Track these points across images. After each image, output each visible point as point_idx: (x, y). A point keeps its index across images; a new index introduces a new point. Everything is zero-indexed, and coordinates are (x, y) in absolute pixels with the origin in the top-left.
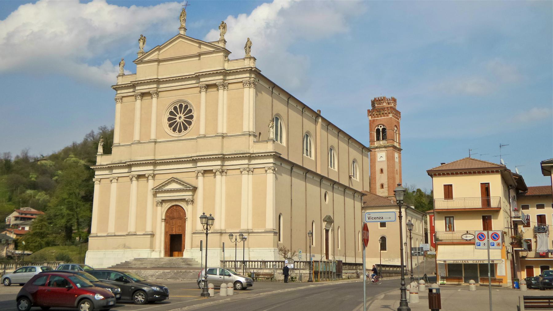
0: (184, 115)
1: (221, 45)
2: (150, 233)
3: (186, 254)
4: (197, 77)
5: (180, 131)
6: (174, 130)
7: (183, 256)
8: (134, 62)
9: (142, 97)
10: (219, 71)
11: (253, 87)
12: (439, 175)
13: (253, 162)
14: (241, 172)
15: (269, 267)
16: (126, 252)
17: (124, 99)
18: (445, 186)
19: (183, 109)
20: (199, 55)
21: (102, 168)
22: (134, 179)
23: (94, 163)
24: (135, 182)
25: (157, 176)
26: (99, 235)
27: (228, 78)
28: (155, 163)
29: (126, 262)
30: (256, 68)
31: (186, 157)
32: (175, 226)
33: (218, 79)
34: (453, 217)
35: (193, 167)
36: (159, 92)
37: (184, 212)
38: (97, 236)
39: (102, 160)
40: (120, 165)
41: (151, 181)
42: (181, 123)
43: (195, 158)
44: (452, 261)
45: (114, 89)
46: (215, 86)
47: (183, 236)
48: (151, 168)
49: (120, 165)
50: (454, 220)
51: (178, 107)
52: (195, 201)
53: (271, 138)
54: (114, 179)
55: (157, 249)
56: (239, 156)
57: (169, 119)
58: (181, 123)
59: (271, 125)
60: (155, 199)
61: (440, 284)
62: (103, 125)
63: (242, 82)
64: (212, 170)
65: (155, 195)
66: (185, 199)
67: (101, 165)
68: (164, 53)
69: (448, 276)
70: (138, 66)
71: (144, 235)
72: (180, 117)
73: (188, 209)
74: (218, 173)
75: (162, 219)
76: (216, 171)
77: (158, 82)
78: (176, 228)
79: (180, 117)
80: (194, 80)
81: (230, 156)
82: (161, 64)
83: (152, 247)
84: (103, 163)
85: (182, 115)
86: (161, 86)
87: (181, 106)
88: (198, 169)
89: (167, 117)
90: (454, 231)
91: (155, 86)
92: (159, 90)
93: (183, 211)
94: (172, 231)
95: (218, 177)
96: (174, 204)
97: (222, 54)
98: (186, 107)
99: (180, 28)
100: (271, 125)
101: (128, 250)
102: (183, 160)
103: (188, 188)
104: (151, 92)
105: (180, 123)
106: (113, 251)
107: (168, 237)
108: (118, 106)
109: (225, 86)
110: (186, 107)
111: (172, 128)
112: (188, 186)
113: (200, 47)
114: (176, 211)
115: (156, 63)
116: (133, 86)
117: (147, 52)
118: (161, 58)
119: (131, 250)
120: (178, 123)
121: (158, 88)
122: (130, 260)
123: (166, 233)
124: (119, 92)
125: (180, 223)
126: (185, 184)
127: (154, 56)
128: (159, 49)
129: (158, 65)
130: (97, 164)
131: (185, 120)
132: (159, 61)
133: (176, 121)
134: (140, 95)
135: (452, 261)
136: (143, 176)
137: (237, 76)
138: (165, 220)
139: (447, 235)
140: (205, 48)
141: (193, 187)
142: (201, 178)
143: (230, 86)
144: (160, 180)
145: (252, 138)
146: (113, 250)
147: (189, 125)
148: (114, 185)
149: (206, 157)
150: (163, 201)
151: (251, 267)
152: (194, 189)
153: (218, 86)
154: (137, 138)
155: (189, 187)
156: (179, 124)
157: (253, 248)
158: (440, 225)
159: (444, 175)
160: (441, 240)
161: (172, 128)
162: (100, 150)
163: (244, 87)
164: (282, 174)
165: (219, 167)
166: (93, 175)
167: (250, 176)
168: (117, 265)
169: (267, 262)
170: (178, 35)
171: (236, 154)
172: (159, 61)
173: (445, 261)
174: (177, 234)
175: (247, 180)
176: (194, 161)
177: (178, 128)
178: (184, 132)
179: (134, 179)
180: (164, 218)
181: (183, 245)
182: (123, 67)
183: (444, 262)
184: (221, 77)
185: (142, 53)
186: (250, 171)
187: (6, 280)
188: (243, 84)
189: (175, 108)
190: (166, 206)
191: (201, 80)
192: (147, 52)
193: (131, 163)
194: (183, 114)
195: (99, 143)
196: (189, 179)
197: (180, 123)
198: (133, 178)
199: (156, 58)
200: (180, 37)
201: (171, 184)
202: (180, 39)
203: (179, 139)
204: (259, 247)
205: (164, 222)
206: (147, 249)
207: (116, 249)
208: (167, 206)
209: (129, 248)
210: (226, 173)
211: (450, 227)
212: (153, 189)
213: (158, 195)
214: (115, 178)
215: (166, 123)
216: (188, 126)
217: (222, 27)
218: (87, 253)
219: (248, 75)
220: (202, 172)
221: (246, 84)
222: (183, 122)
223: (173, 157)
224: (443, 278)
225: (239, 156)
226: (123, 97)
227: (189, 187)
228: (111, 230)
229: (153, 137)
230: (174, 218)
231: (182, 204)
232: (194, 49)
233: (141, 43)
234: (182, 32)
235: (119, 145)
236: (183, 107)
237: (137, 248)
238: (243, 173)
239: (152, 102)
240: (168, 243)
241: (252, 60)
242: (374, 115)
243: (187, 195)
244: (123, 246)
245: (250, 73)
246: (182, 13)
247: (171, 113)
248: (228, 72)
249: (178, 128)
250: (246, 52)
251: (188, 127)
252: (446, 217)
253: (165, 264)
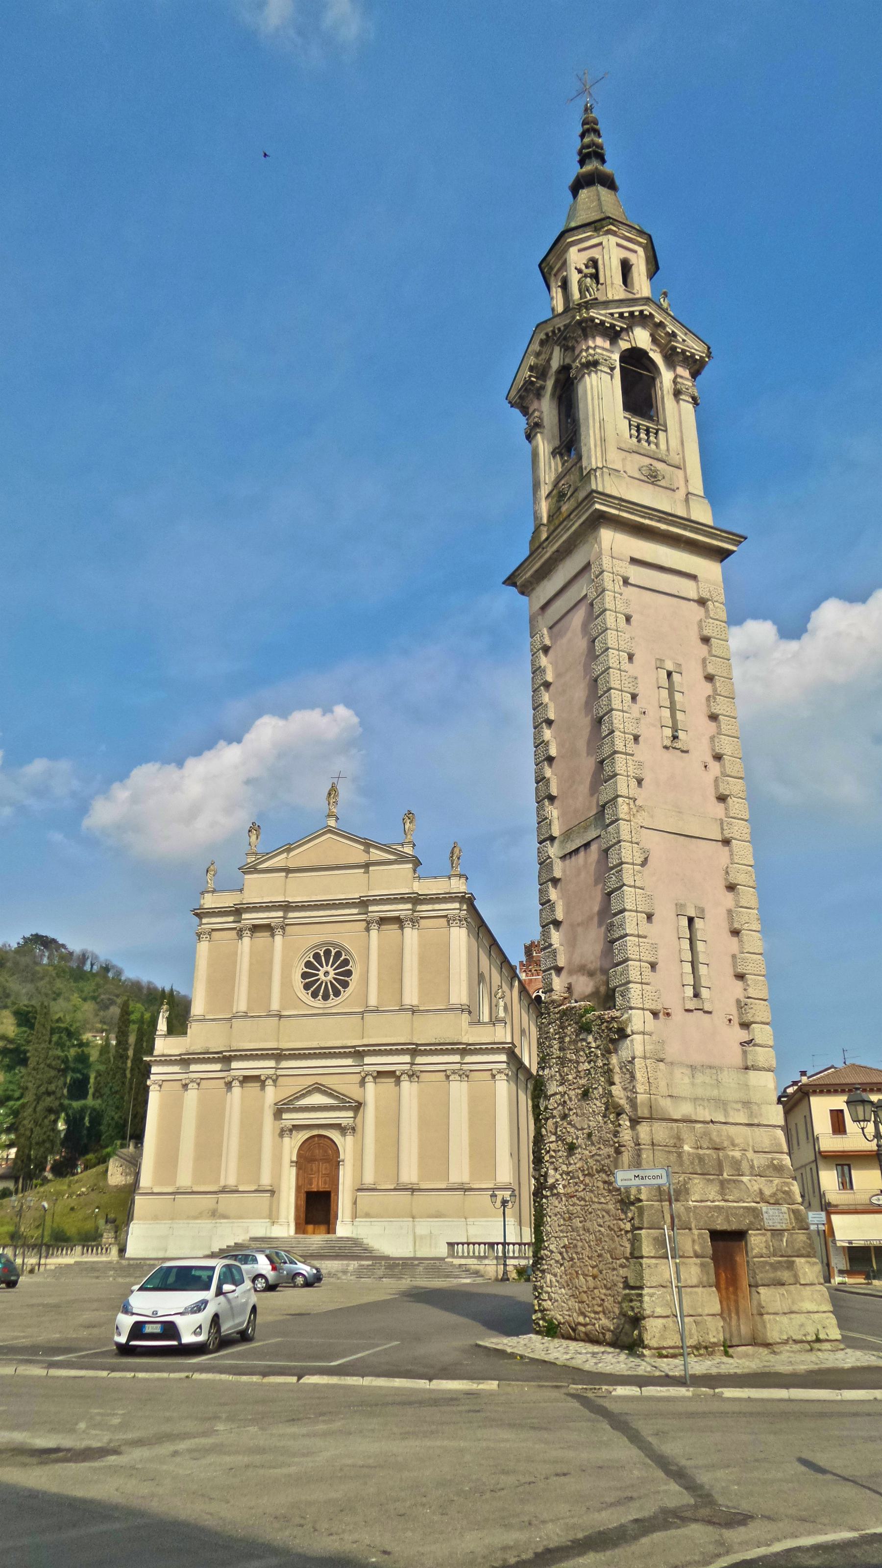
0: (335, 970)
1: (408, 850)
2: (269, 1188)
3: (343, 1229)
4: (363, 904)
5: (326, 997)
6: (315, 995)
7: (335, 1233)
8: (239, 869)
9: (253, 932)
10: (406, 896)
11: (465, 925)
12: (821, 1092)
13: (469, 1059)
14: (448, 1077)
15: (460, 1254)
16: (218, 1225)
17: (214, 933)
18: (831, 1111)
19: (323, 958)
20: (366, 866)
21: (167, 1060)
22: (236, 1083)
23: (150, 1051)
24: (237, 1090)
25: (280, 1078)
26: (155, 1191)
27: (419, 908)
28: (279, 1056)
29: (235, 1244)
30: (472, 894)
31: (340, 1045)
32: (316, 1175)
33: (402, 909)
34: (849, 1166)
35: (354, 1064)
36: (287, 925)
37: (335, 1148)
38: (153, 1194)
39: (163, 1045)
40: (206, 1056)
41: (270, 1089)
42: (329, 984)
43: (361, 1049)
44: (863, 1242)
45: (197, 915)
46: (398, 921)
47: (332, 1195)
48: (272, 1063)
49: (206, 1056)
50: (853, 1172)
51: (322, 953)
52: (359, 1129)
53: (501, 1017)
54: (192, 1081)
55: (282, 1220)
56: (444, 1047)
57: (304, 975)
58: (329, 984)
59: (500, 994)
60: (277, 1122)
61: (839, 1284)
62: (151, 980)
63: (446, 916)
64: (394, 1072)
65: (278, 1114)
66: (340, 1124)
67: (163, 1056)
68: (295, 859)
69: (849, 1269)
70: (247, 877)
71: (256, 1191)
72: (326, 973)
73: (346, 1145)
74: (404, 1077)
75: (292, 1162)
76: (402, 1074)
77: (287, 907)
78: (318, 1180)
79: (326, 973)
80: (355, 907)
81: (428, 1048)
82: (290, 875)
83: (273, 1217)
84: (167, 1052)
85: (329, 969)
86: (291, 915)
87: (327, 953)
88: (366, 1068)
89: (301, 972)
90: (852, 1188)
91: (280, 914)
92: (287, 921)
93: (334, 1146)
94: (311, 1184)
95: (405, 1085)
96: (315, 1132)
97: (411, 866)
98: (338, 955)
99: (329, 816)
100: (500, 994)
101: (222, 1221)
102: (337, 1051)
103: (347, 1105)
104: (272, 925)
105: (326, 983)
106: (189, 1223)
107: (303, 1196)
108: (203, 947)
109: (414, 922)
110: (338, 955)
111: (310, 992)
112: (348, 1100)
113: (368, 853)
114: (319, 1146)
115: (284, 874)
116: (237, 912)
117: (268, 854)
118: (291, 865)
119: (231, 1221)
120: (322, 983)
121: (285, 918)
122: (244, 1241)
123: (298, 1188)
124: (204, 921)
125: (326, 1168)
126: (342, 1097)
127: (278, 861)
128: (289, 850)
129: (286, 877)
130: (156, 1053)
131: (335, 979)
132: (288, 871)
133: (319, 979)
134: (250, 929)
135: (863, 1242)
136: (256, 1078)
137: (437, 907)
138: (297, 1162)
139: (843, 1196)
140: (376, 855)
141: (356, 1102)
142: (370, 1086)
143: (422, 922)
144: (289, 1087)
145: (465, 1015)
146: (188, 1221)
147: (343, 988)
148: (192, 1095)
149: (383, 1048)
150: (297, 1128)
151: (471, 1254)
152: (358, 1107)
153: (403, 922)
154: (242, 1005)
155: (349, 1102)
156: (324, 984)
157: (474, 1217)
158: (829, 1179)
159: (829, 1092)
160: (836, 1206)
161: (310, 992)
162: (162, 1026)
163: (449, 925)
164: (511, 1082)
165: (407, 1067)
166: (147, 1073)
167: (464, 1084)
168: (220, 1250)
169: (458, 1244)
170: (325, 828)
171: (440, 1044)
172: (288, 871)
173: (850, 1242)
174: (321, 1190)
175: (458, 1090)
176: (358, 1054)
177: (322, 991)
178: (333, 1001)
179: (236, 1083)
180: (294, 1159)
181: (332, 1213)
182: (214, 875)
183: (849, 1243)
184: (409, 906)
185: (256, 854)
186: (464, 1075)
187: (260, 1279)
188: (448, 921)
189: (317, 956)
190: (300, 1136)
191: (371, 909)
192: (268, 854)
193: (233, 1054)
194: (331, 967)
195: (161, 1014)
196: (349, 1087)
197: (326, 983)
198: (234, 1082)
199: (282, 864)
200: (330, 831)
201: (311, 1095)
202: (329, 835)
203: (326, 1011)
204: (484, 1217)
205: (295, 1168)
206: (264, 1218)
207: (195, 1218)
208: (302, 1136)
209: (225, 1217)
210: (418, 1077)
211: (846, 1184)
212: (275, 1104)
213: (285, 1116)
214: (195, 1081)
215: (298, 982)
216: (342, 990)
217: (408, 821)
218: (131, 1225)
219: (457, 905)
220: (241, 1078)
221: (454, 920)
222: (331, 982)
223: (338, 1043)
224: (841, 1272)
225: (444, 1047)
226: (213, 930)
227: (349, 1102)
228: (184, 1179)
229: (275, 1006)
230: (315, 1160)
231: (335, 1135)
232: (356, 853)
233: (254, 838)
234: (332, 823)
235: (203, 1020)
236: (333, 954)
237: (241, 1217)
238: (450, 1079)
239: (273, 946)
240: (303, 1209)
241: (463, 880)
242: (530, 971)
243: (344, 1117)
244: (210, 1214)
245: (460, 903)
246: (330, 790)
247: (308, 964)
248: (421, 897)
249: (322, 991)
250: (452, 864)
251: (342, 992)
252: (837, 1165)
253: (322, 1248)
